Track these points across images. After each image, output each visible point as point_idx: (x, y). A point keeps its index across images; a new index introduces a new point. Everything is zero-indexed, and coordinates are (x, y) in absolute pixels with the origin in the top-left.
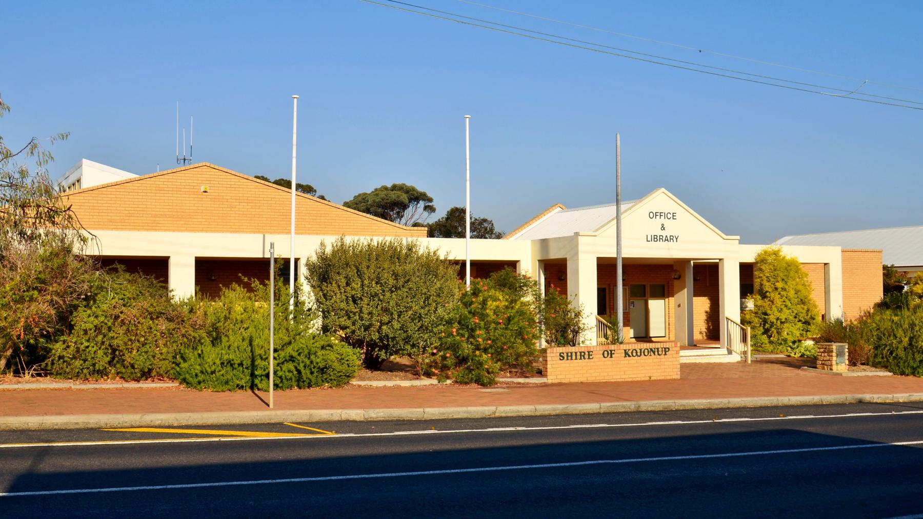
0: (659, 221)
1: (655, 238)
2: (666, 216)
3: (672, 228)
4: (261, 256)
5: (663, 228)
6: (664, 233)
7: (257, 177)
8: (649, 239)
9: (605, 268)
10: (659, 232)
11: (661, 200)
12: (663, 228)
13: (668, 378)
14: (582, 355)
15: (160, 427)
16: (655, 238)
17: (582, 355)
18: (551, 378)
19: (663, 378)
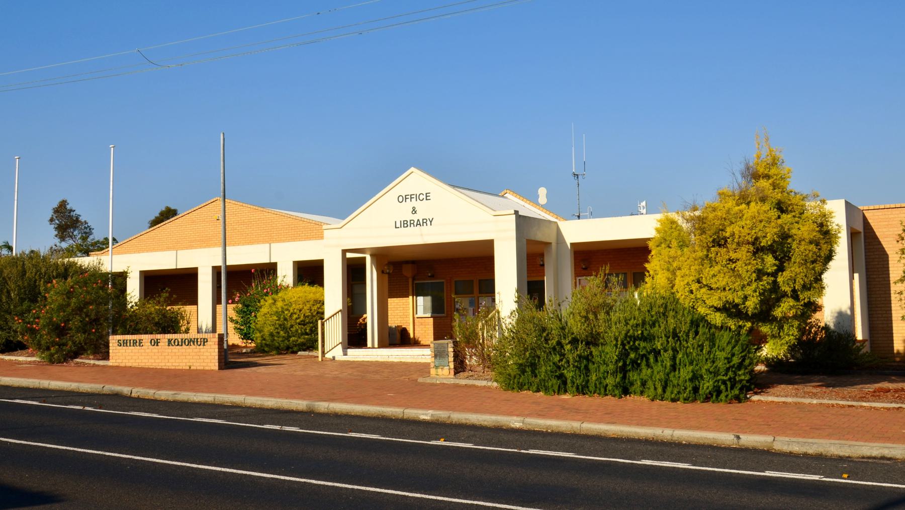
0: (409, 205)
1: (405, 224)
2: (418, 197)
3: (424, 210)
4: (268, 261)
5: (414, 211)
6: (415, 217)
7: (156, 222)
8: (398, 225)
9: (216, 271)
10: (409, 217)
11: (415, 180)
12: (414, 211)
13: (207, 368)
14: (191, 342)
15: (323, 329)
16: (405, 224)
17: (191, 342)
18: (111, 363)
19: (202, 368)
